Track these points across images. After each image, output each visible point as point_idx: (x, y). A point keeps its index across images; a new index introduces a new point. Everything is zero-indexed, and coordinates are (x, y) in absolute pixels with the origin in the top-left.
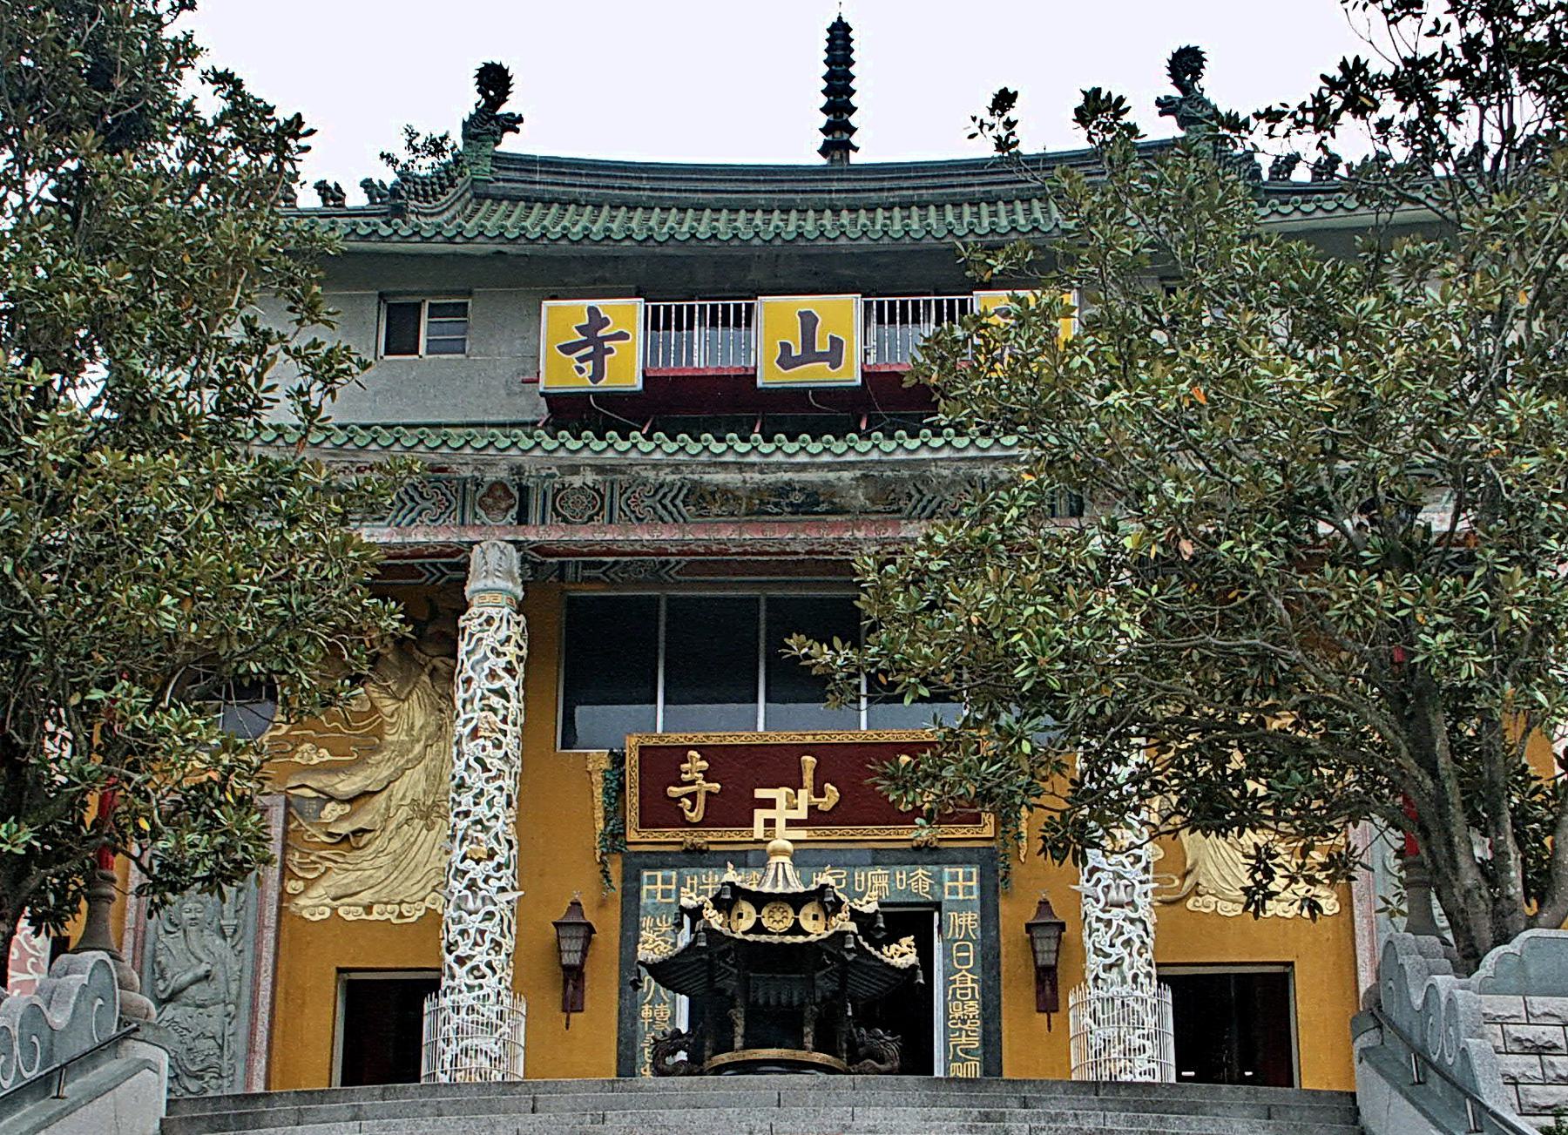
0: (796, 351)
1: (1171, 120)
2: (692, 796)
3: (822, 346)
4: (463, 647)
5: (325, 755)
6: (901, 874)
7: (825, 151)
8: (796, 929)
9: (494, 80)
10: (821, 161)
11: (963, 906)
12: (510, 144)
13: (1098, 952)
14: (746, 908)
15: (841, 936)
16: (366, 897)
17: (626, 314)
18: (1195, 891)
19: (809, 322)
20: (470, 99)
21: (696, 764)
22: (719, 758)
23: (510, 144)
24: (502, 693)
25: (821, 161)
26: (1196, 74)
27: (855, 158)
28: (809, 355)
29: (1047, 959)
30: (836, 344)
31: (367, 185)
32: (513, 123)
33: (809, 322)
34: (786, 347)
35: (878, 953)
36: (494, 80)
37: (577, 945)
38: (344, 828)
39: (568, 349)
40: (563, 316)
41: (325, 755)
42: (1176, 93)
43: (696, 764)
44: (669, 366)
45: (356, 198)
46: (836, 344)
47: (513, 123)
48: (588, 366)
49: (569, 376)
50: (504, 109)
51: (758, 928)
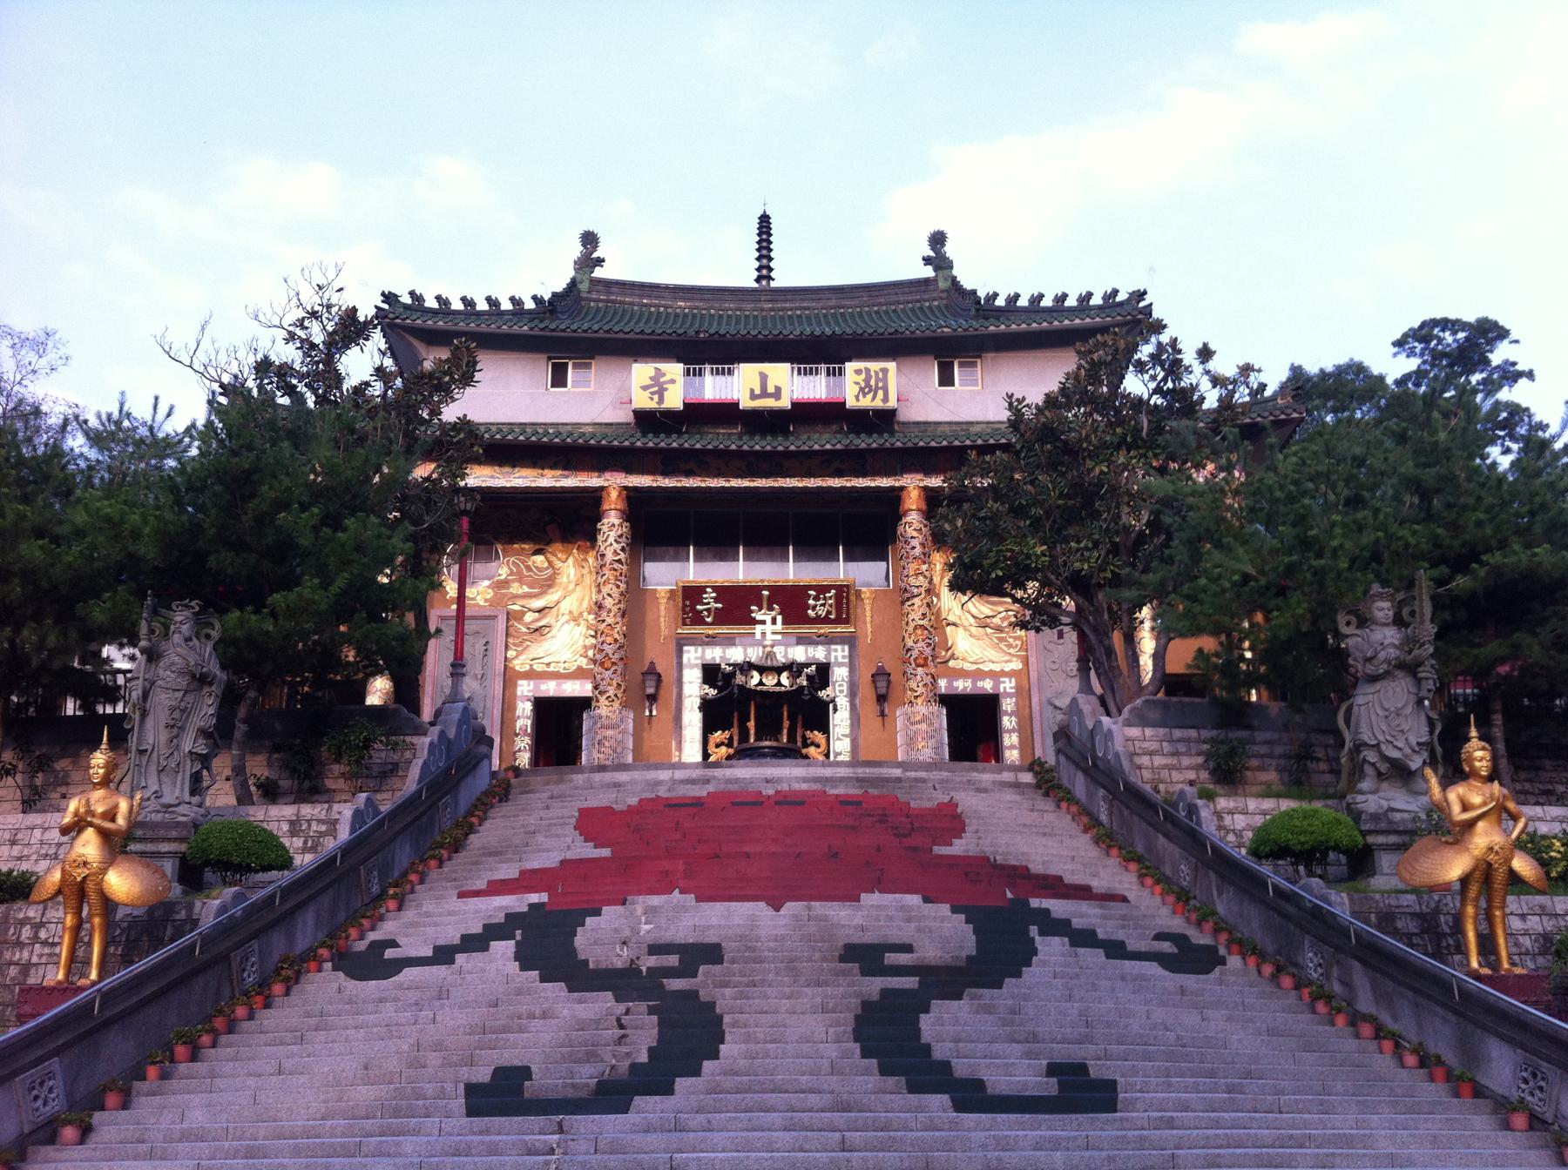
0: (758, 391)
1: (930, 268)
2: (708, 610)
3: (771, 389)
4: (600, 538)
5: (526, 589)
6: (811, 649)
7: (758, 280)
8: (779, 684)
9: (590, 240)
10: (756, 285)
11: (840, 665)
12: (598, 273)
13: (912, 690)
14: (756, 674)
15: (801, 688)
16: (546, 660)
17: (674, 370)
18: (953, 657)
19: (764, 378)
20: (577, 250)
21: (710, 595)
22: (723, 592)
23: (598, 273)
24: (619, 561)
25: (756, 285)
26: (943, 245)
27: (773, 284)
28: (764, 394)
29: (882, 691)
30: (778, 389)
31: (534, 298)
32: (600, 262)
33: (764, 378)
34: (752, 391)
35: (1215, 893)
36: (590, 240)
37: (653, 683)
38: (534, 626)
39: (645, 388)
40: (642, 371)
41: (526, 589)
42: (932, 254)
43: (710, 595)
44: (694, 397)
45: (530, 305)
46: (778, 389)
47: (600, 262)
48: (656, 397)
49: (644, 401)
50: (595, 255)
51: (761, 683)
